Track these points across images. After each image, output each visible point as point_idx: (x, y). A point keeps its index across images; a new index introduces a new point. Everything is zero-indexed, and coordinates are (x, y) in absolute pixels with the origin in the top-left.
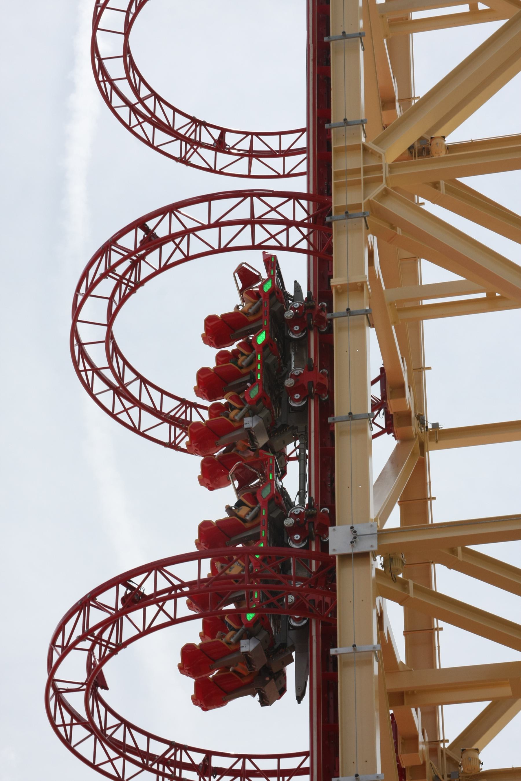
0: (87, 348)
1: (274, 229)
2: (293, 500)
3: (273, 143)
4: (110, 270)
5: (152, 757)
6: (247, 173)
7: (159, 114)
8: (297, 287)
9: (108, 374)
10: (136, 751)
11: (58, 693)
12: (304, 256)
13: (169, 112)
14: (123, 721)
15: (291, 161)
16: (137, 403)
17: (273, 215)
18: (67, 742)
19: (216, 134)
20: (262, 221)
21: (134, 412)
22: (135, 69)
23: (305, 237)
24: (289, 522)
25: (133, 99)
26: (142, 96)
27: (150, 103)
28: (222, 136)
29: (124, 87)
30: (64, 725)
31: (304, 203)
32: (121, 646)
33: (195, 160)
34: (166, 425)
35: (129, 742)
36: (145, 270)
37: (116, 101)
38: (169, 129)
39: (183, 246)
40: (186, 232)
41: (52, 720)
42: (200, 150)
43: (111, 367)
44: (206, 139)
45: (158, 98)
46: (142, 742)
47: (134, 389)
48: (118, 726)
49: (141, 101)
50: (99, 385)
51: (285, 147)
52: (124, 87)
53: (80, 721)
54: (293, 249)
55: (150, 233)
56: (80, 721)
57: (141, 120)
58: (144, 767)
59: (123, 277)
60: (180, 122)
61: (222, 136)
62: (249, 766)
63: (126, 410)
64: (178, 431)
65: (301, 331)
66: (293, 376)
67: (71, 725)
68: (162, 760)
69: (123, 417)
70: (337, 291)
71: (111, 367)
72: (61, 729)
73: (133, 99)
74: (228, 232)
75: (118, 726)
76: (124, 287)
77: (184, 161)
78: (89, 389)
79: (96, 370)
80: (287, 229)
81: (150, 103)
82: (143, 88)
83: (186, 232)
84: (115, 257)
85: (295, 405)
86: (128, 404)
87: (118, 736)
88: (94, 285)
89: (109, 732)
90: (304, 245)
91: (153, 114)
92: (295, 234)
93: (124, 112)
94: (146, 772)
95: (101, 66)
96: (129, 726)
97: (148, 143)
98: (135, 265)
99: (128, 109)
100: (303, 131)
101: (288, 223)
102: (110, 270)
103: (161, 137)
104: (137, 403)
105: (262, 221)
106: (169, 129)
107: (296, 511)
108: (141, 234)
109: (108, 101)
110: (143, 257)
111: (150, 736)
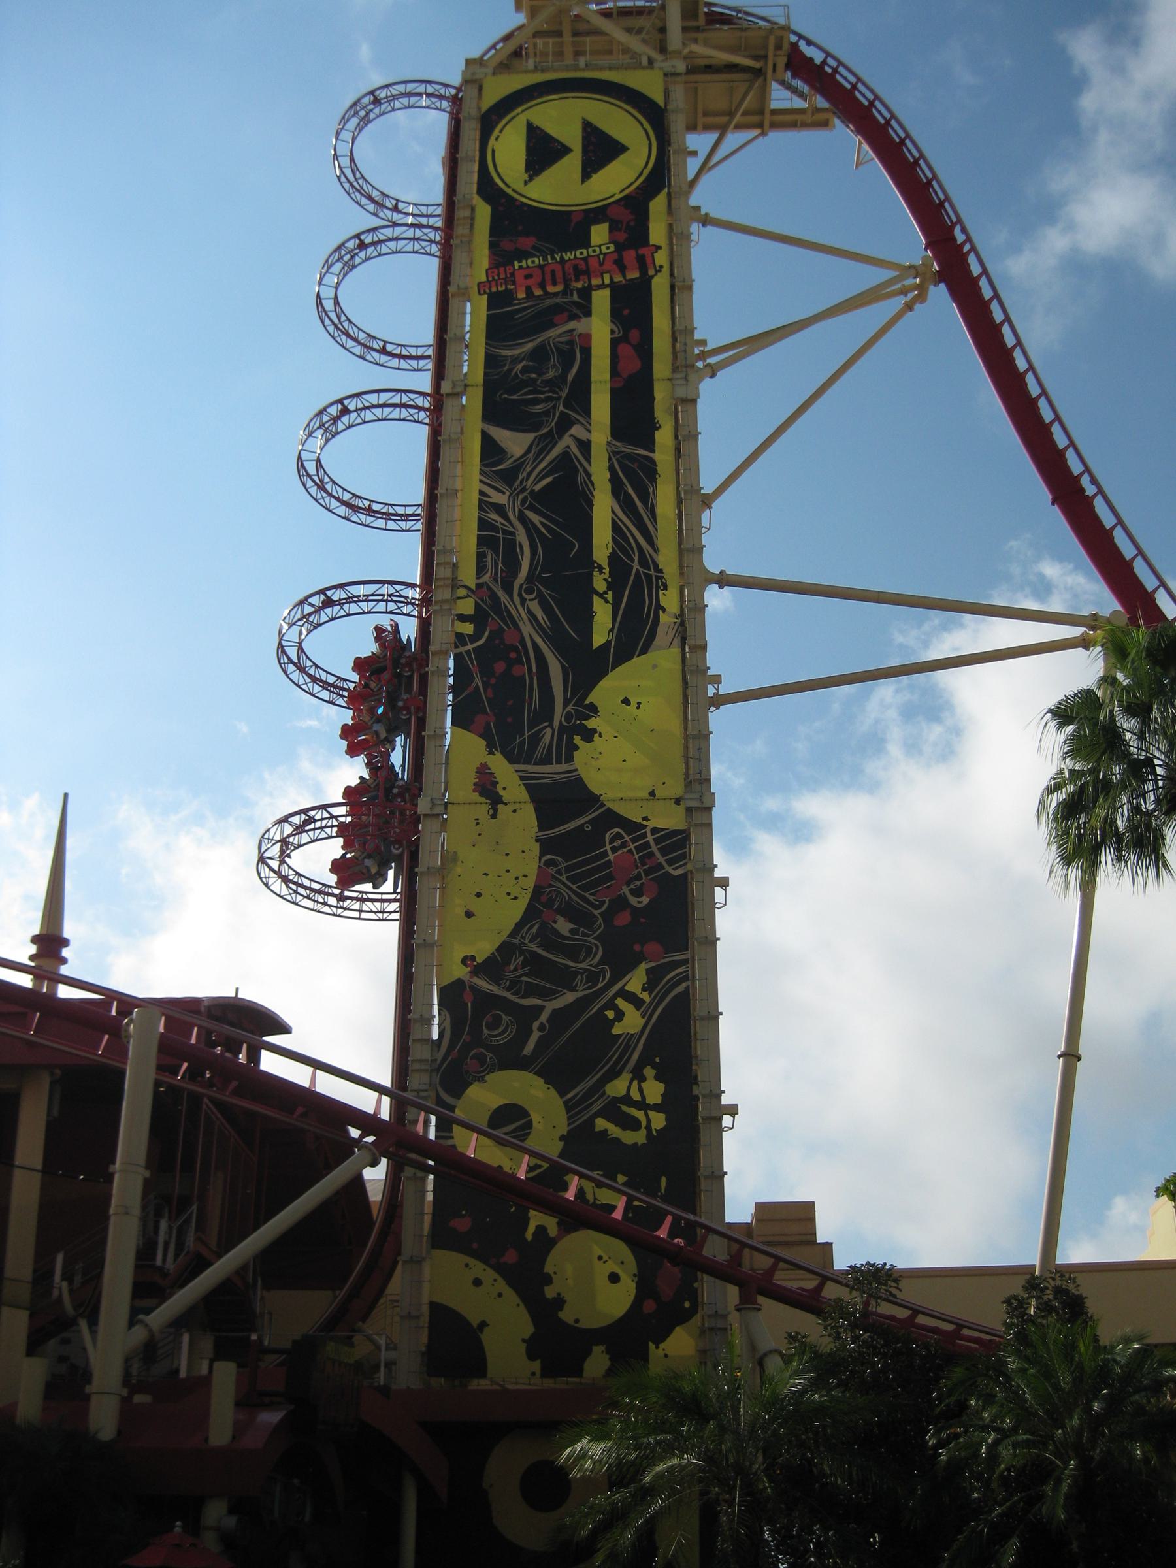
0: (305, 463)
1: (424, 243)
2: (397, 771)
3: (413, 351)
4: (341, 258)
5: (328, 684)
6: (397, 367)
7: (351, 332)
8: (409, 639)
9: (316, 478)
10: (320, 680)
11: (282, 647)
12: (427, 427)
13: (356, 330)
14: (314, 664)
15: (422, 363)
16: (330, 495)
17: (425, 237)
18: (285, 672)
19: (394, 202)
20: (418, 239)
21: (327, 499)
22: (340, 306)
23: (428, 416)
24: (395, 791)
25: (336, 321)
26: (342, 320)
27: (346, 324)
28: (396, 204)
29: (333, 316)
30: (284, 663)
31: (429, 398)
32: (337, 433)
33: (369, 357)
34: (344, 507)
35: (317, 676)
36: (358, 260)
37: (327, 322)
38: (355, 340)
39: (378, 249)
40: (380, 242)
41: (279, 660)
42: (385, 210)
43: (318, 475)
44: (389, 205)
45: (350, 322)
46: (323, 676)
47: (329, 487)
48: (311, 666)
49: (356, 180)
50: (310, 483)
51: (419, 354)
52: (333, 316)
53: (292, 662)
54: (421, 422)
55: (362, 242)
56: (292, 662)
57: (340, 333)
58: (325, 688)
59: (347, 263)
60: (375, 194)
61: (396, 204)
62: (365, 896)
63: (323, 498)
64: (350, 511)
65: (409, 671)
66: (403, 700)
67: (288, 663)
68: (332, 685)
69: (321, 501)
70: (432, 654)
71: (318, 475)
72: (283, 665)
73: (336, 321)
74: (401, 243)
75: (311, 666)
76: (346, 268)
77: (362, 357)
78: (304, 485)
79: (308, 475)
80: (418, 413)
81: (346, 324)
82: (343, 316)
83: (380, 242)
84: (343, 253)
85: (404, 717)
86: (324, 495)
87: (312, 672)
88: (332, 265)
89: (307, 669)
90: (438, 254)
91: (362, 188)
92: (422, 415)
93: (331, 329)
94: (325, 691)
95: (321, 302)
96: (317, 666)
97: (343, 346)
98: (352, 258)
99: (333, 327)
100: (429, 346)
101: (431, 242)
102: (341, 258)
103: (350, 343)
104: (330, 495)
105: (418, 239)
106: (355, 340)
107: (401, 783)
108: (357, 241)
109: (323, 322)
110: (357, 254)
111: (328, 673)
